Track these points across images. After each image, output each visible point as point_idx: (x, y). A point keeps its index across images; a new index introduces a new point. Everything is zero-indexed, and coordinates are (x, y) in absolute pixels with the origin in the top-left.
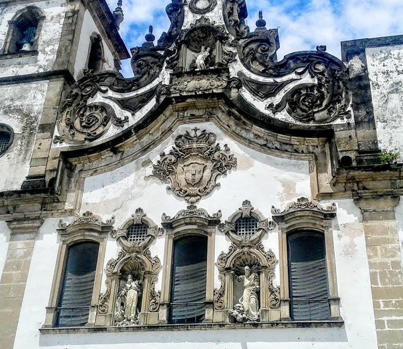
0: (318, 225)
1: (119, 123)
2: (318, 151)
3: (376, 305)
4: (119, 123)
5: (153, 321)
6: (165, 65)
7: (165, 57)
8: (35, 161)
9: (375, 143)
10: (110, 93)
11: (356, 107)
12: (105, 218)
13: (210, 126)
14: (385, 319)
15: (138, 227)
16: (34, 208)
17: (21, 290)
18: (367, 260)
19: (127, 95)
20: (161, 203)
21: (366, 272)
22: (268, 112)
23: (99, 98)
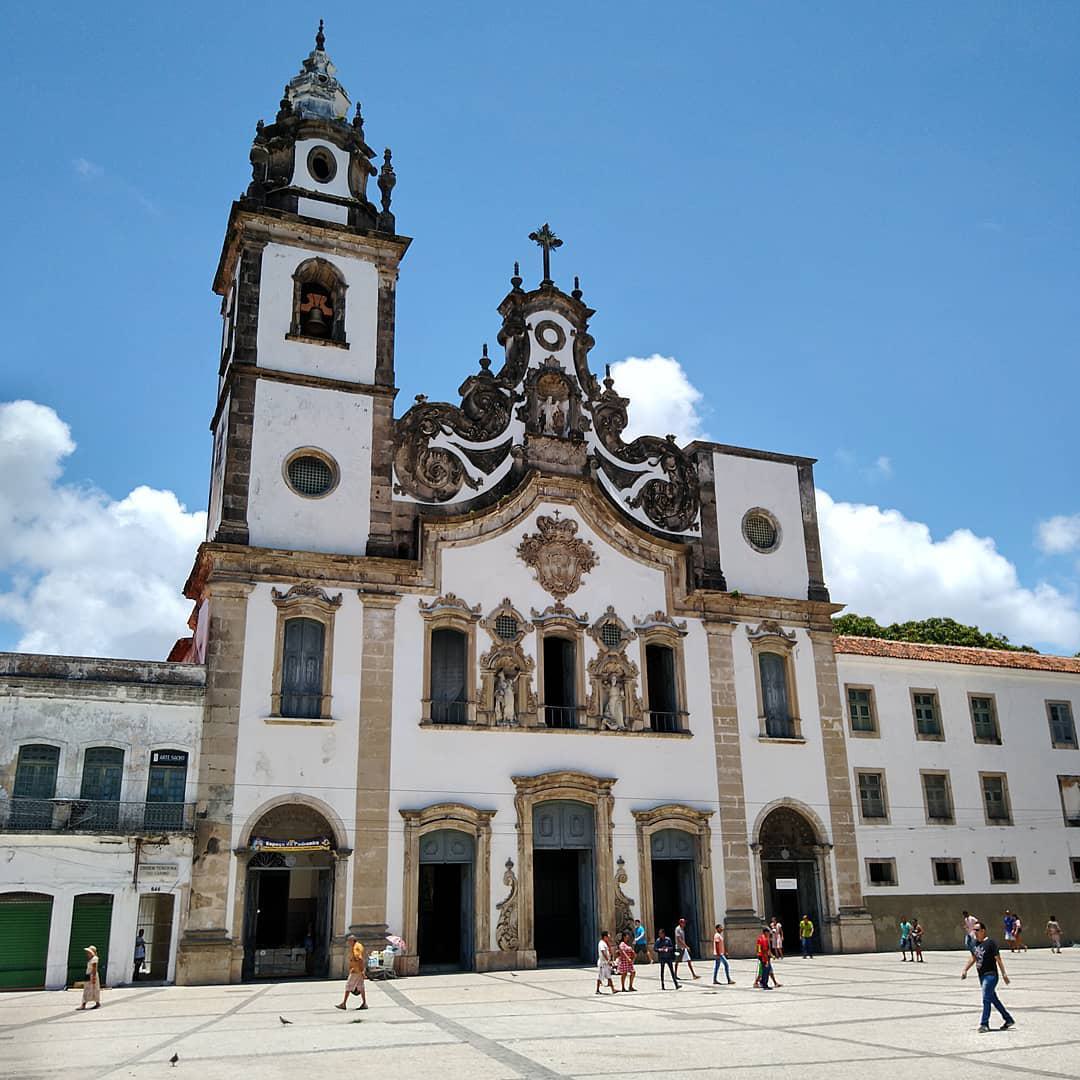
3: (716, 722)
4: (474, 484)
10: (455, 438)
14: (722, 734)
17: (388, 678)
18: (709, 679)
20: (531, 598)
23: (440, 441)
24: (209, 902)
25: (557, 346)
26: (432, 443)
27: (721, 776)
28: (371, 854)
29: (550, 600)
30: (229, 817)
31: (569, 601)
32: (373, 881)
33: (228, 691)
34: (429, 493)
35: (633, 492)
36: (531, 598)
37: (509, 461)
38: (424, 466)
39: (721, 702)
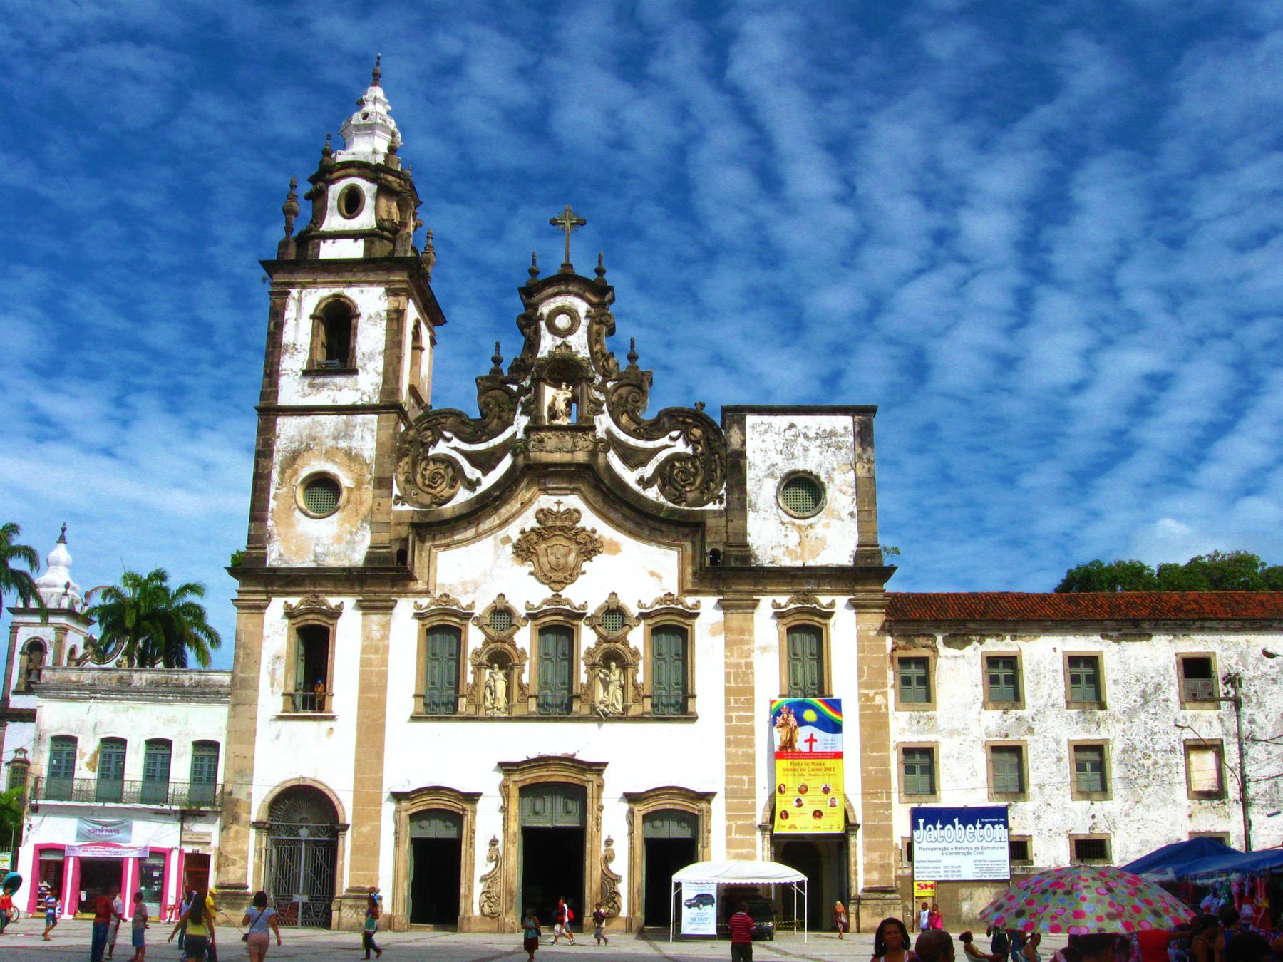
3: (727, 702)
4: (471, 485)
8: (375, 526)
10: (456, 442)
12: (464, 602)
17: (383, 676)
20: (526, 591)
23: (441, 448)
24: (234, 862)
25: (570, 331)
26: (432, 452)
27: (728, 757)
28: (366, 829)
29: (547, 593)
30: (250, 795)
31: (567, 593)
32: (368, 850)
33: (249, 692)
34: (427, 499)
35: (648, 471)
36: (526, 591)
37: (506, 463)
38: (423, 476)
39: (736, 681)
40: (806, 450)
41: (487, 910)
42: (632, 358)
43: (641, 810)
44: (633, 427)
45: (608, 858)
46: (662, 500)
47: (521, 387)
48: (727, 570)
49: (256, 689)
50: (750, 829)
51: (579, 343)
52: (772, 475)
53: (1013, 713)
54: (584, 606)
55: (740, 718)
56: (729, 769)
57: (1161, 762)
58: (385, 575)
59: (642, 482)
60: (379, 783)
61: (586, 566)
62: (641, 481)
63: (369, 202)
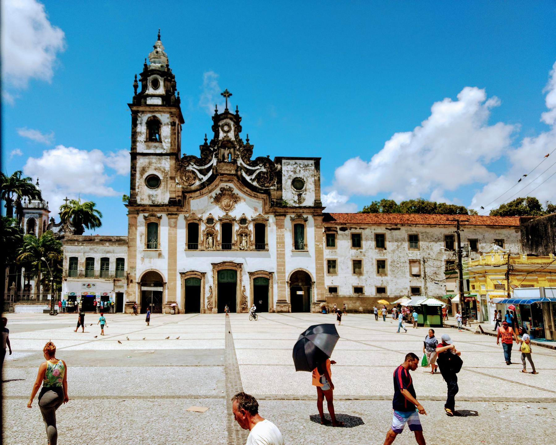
0: (264, 223)
1: (200, 180)
2: (265, 198)
5: (218, 249)
6: (214, 156)
7: (213, 152)
8: (171, 192)
9: (282, 197)
10: (195, 166)
11: (277, 183)
13: (231, 185)
15: (210, 220)
16: (174, 209)
17: (176, 237)
19: (203, 168)
20: (217, 212)
21: (275, 237)
22: (250, 182)
23: (190, 168)
24: (131, 295)
25: (228, 132)
26: (187, 168)
27: (278, 262)
30: (135, 274)
33: (134, 243)
35: (253, 177)
37: (210, 173)
40: (300, 171)
41: (209, 307)
42: (248, 140)
43: (253, 277)
44: (248, 163)
45: (244, 291)
46: (257, 185)
47: (214, 149)
48: (278, 207)
49: (136, 242)
50: (284, 283)
51: (231, 135)
52: (290, 178)
53: (359, 250)
54: (235, 217)
55: (281, 251)
56: (278, 265)
57: (402, 265)
58: (177, 204)
59: (253, 180)
60: (175, 270)
61: (236, 205)
62: (251, 179)
63: (162, 83)
